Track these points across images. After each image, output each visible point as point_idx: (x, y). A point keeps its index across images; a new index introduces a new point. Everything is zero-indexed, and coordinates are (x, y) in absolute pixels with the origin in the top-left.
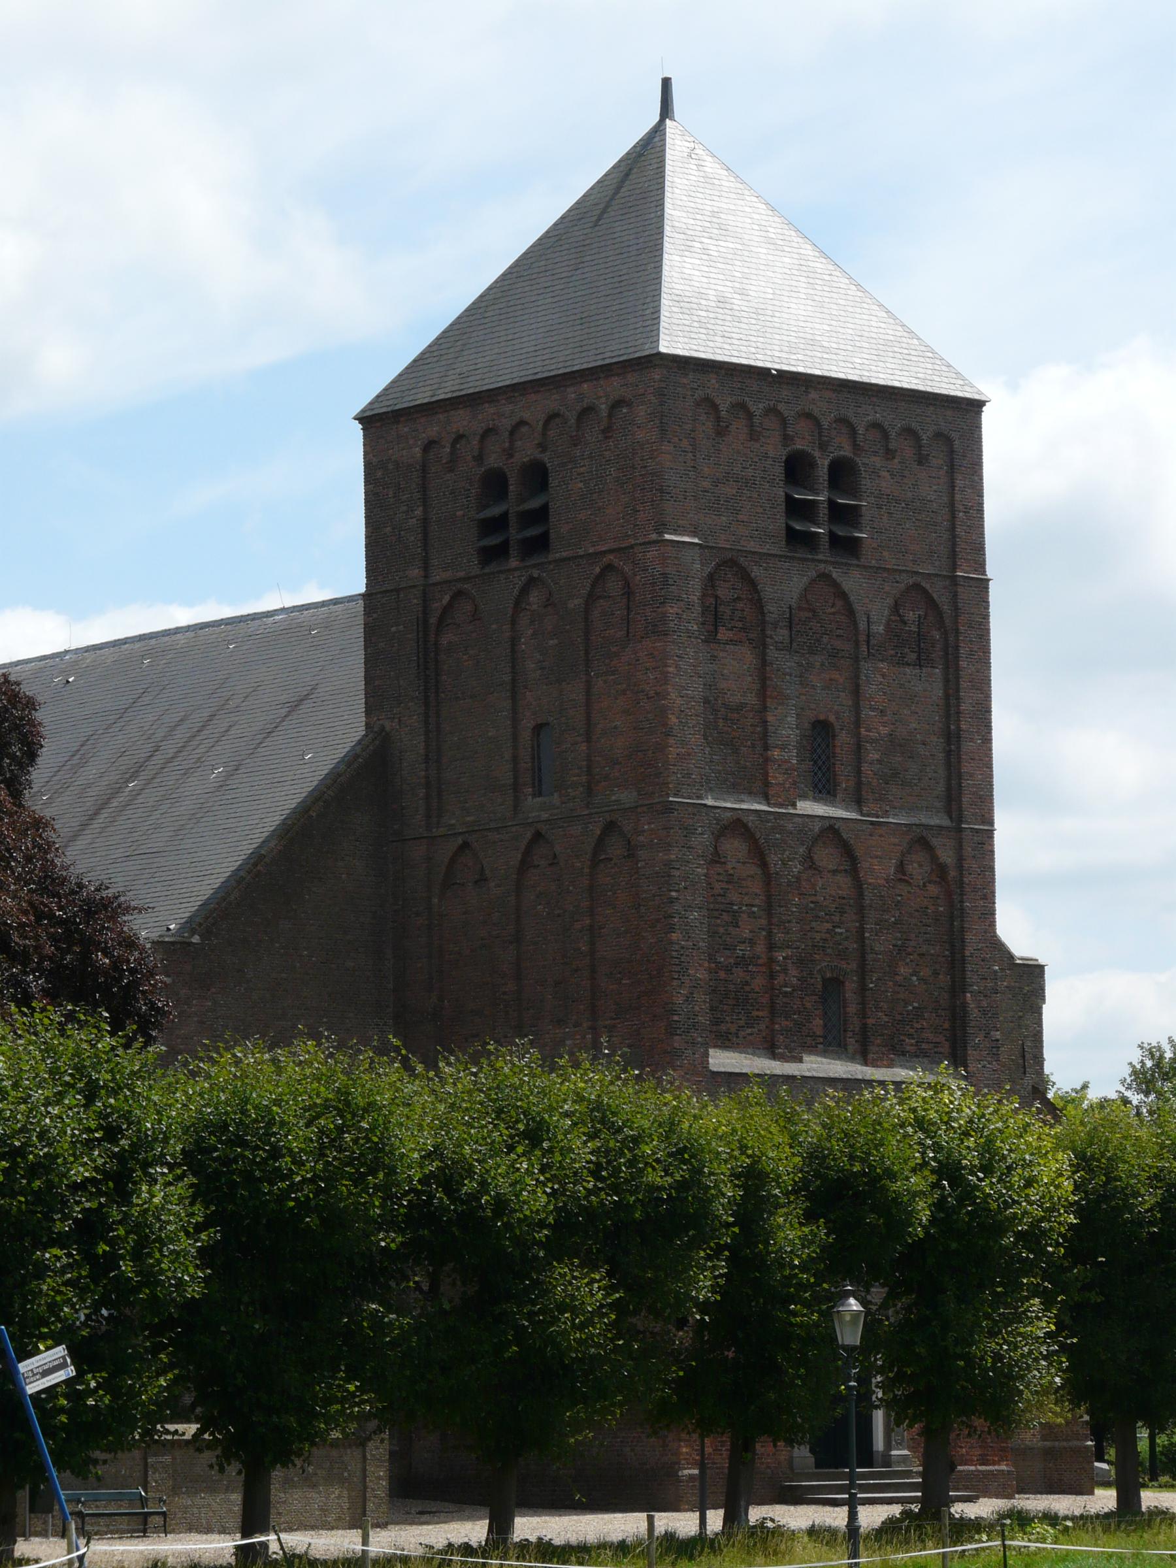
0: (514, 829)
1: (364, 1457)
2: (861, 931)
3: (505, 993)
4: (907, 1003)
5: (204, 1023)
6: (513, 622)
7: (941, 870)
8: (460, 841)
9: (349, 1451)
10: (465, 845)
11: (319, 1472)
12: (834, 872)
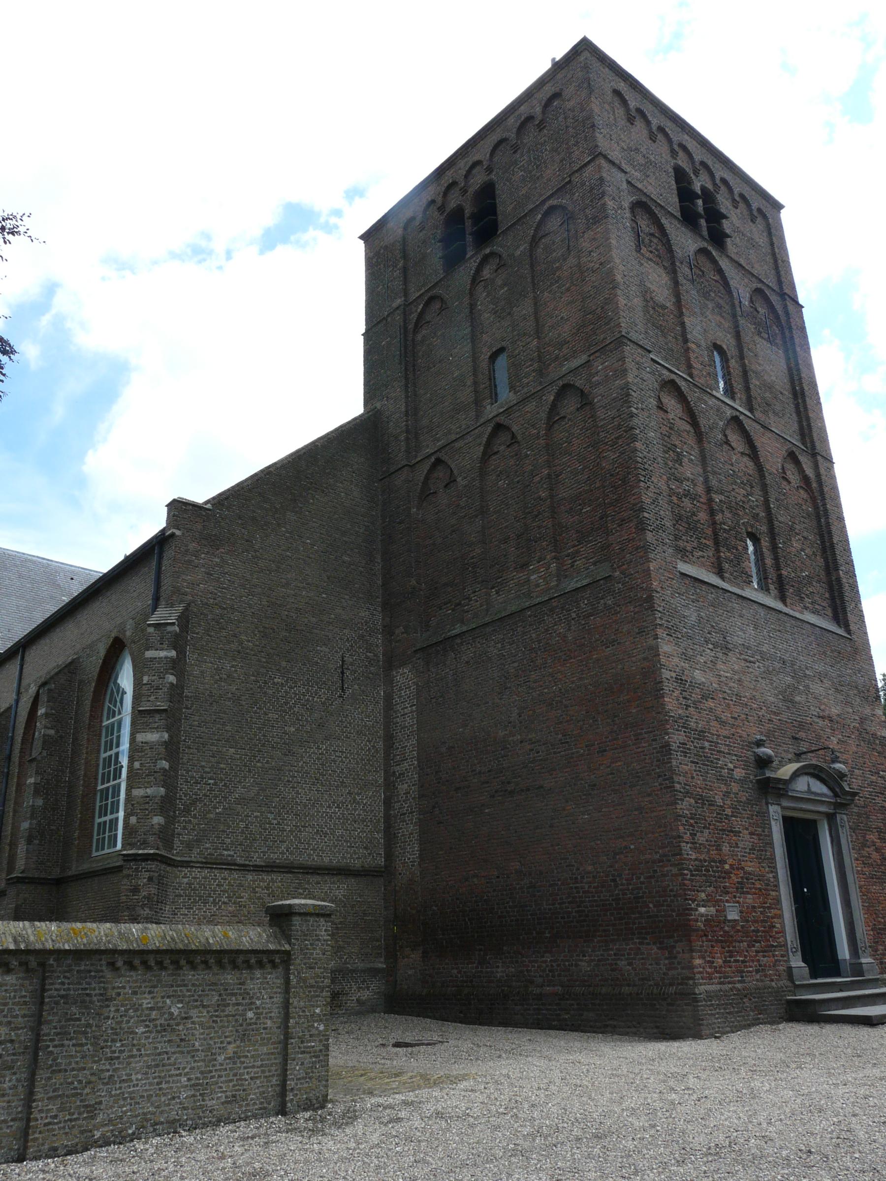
0: (477, 431)
1: (287, 981)
2: (767, 502)
3: (472, 558)
4: (802, 571)
5: (211, 575)
6: (471, 294)
7: (806, 479)
8: (433, 459)
9: (258, 973)
10: (439, 461)
11: (194, 1013)
12: (742, 453)
